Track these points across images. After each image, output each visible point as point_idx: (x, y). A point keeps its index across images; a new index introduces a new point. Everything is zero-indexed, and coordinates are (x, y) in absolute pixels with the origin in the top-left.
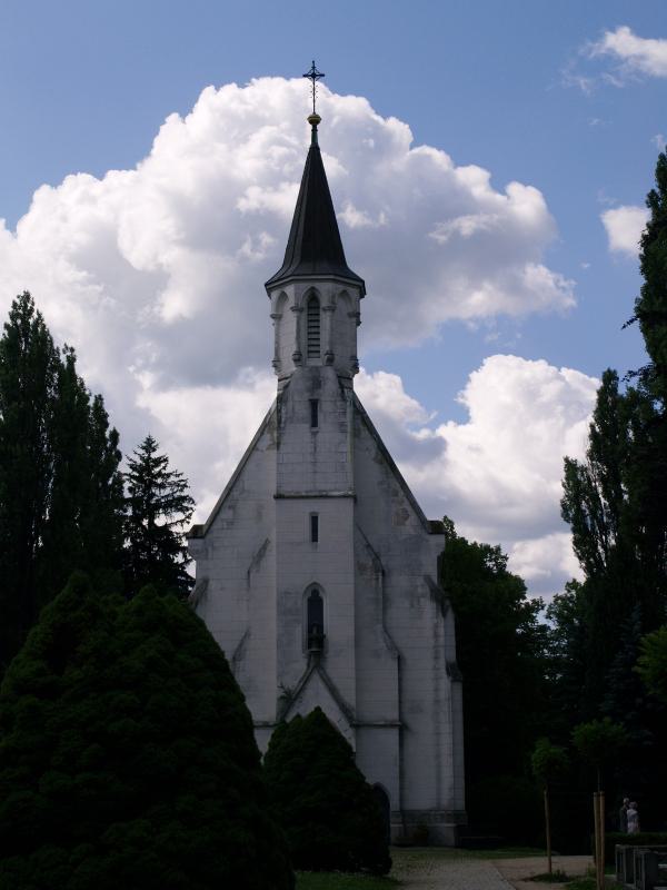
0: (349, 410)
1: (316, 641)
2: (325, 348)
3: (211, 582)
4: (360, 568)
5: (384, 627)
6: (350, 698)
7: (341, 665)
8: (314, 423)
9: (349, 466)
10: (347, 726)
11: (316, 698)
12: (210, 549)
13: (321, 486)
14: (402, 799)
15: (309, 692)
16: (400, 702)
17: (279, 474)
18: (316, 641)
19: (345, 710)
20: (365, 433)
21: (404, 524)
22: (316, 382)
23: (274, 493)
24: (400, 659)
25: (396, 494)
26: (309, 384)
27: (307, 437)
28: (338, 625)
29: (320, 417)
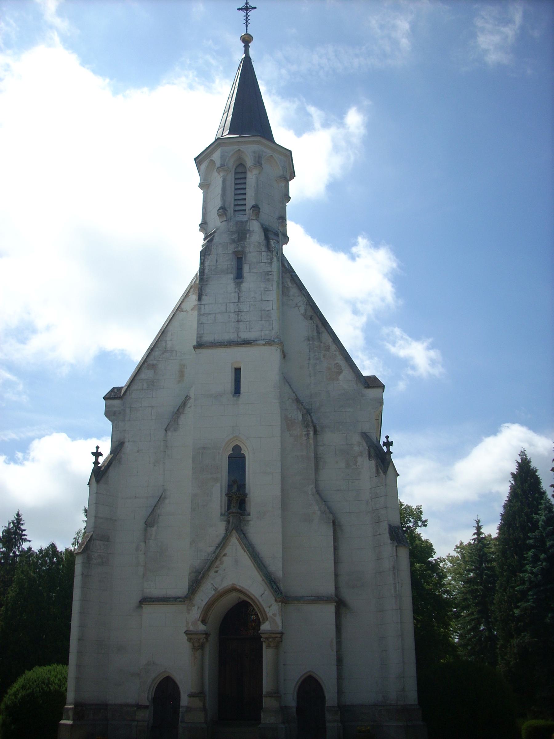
0: (276, 265)
1: (237, 501)
2: (250, 202)
3: (127, 444)
4: (287, 424)
5: (317, 486)
6: (276, 568)
7: (265, 529)
8: (239, 276)
9: (275, 315)
10: (272, 599)
11: (239, 574)
12: (128, 411)
13: (245, 335)
14: (340, 692)
15: (227, 561)
16: (336, 575)
17: (200, 324)
18: (237, 501)
19: (271, 581)
20: (294, 291)
21: (338, 380)
22: (241, 234)
23: (185, 629)
24: (336, 525)
25: (328, 348)
26: (235, 236)
27: (231, 286)
28: (262, 486)
29: (246, 268)
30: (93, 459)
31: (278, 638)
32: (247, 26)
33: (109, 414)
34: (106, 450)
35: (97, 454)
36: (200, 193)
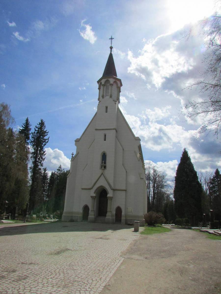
11: (102, 183)
30: (72, 155)
31: (111, 198)
32: (111, 44)
33: (76, 145)
34: (75, 153)
35: (73, 154)
36: (98, 90)
